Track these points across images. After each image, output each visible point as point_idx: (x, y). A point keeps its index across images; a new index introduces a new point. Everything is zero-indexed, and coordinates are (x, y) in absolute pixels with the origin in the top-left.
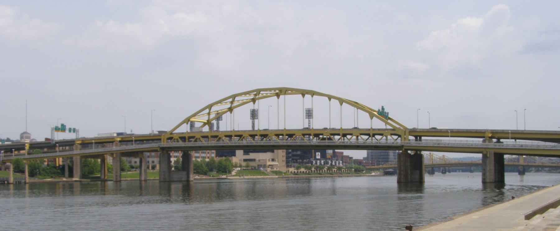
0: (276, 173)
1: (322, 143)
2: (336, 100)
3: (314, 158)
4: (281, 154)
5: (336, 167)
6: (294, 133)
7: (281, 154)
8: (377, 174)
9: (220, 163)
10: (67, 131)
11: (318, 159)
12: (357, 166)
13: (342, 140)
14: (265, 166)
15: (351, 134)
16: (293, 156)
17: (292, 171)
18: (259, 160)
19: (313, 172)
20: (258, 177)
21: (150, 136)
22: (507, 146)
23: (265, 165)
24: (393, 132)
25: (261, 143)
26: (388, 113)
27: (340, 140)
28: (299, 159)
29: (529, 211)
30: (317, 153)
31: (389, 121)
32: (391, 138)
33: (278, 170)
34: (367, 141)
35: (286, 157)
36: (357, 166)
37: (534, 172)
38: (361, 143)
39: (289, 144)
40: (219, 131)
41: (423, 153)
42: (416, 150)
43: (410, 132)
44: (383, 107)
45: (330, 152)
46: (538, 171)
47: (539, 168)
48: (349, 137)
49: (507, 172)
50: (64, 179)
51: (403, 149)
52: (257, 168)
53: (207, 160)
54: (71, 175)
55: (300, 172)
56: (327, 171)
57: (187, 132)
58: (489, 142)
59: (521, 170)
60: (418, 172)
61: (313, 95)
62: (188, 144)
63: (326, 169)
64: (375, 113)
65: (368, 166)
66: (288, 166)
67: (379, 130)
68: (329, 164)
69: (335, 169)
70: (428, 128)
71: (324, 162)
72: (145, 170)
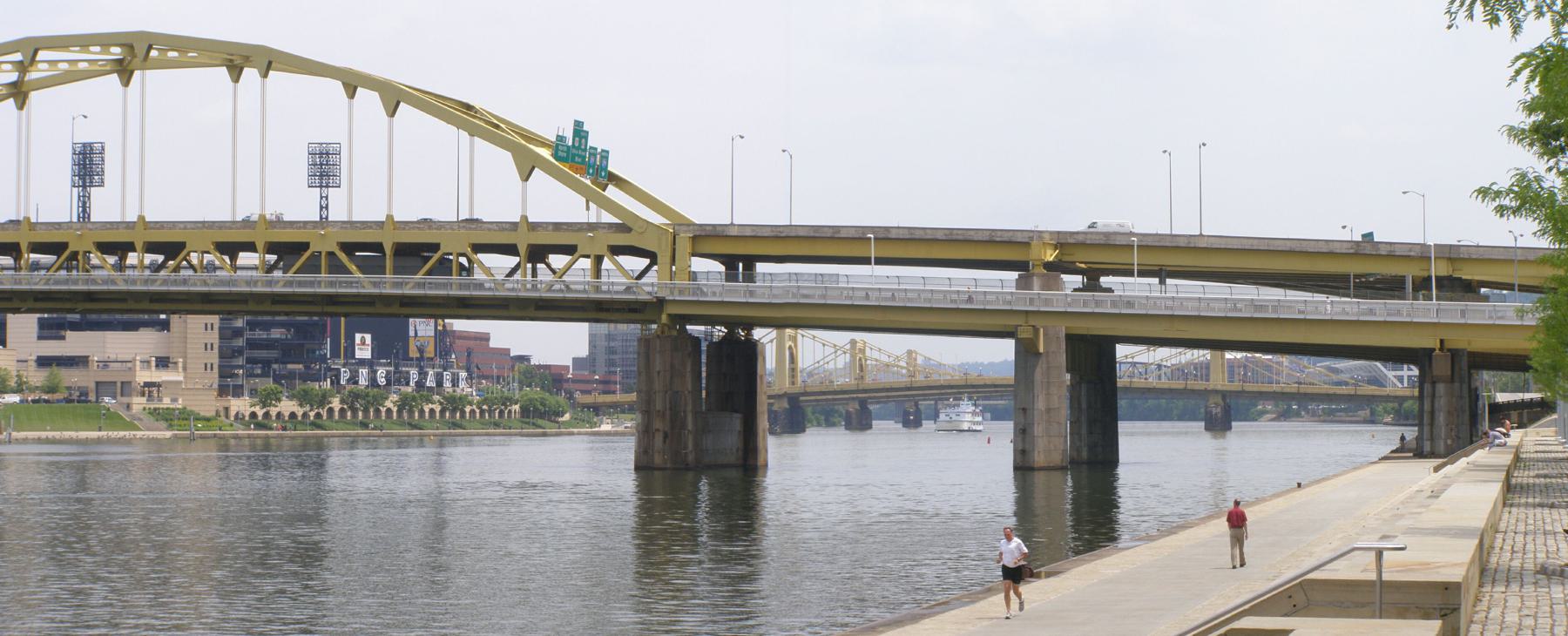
0: (167, 417)
1: (300, 284)
8: (621, 429)
11: (362, 362)
13: (525, 275)
14: (126, 388)
15: (569, 250)
16: (252, 345)
17: (242, 409)
18: (105, 364)
20: (83, 435)
22: (824, 297)
23: (129, 383)
25: (154, 281)
26: (605, 155)
27: (518, 276)
28: (276, 361)
29: (19, 359)
30: (358, 337)
31: (612, 192)
33: (180, 404)
34: (644, 280)
36: (535, 393)
41: (758, 333)
44: (578, 125)
45: (422, 329)
46: (1284, 415)
48: (557, 261)
51: (664, 318)
52: (92, 397)
55: (279, 415)
56: (400, 412)
58: (1046, 286)
59: (1217, 411)
60: (736, 421)
61: (269, 66)
64: (545, 153)
65: (589, 392)
66: (223, 391)
67: (558, 226)
69: (433, 406)
71: (387, 378)
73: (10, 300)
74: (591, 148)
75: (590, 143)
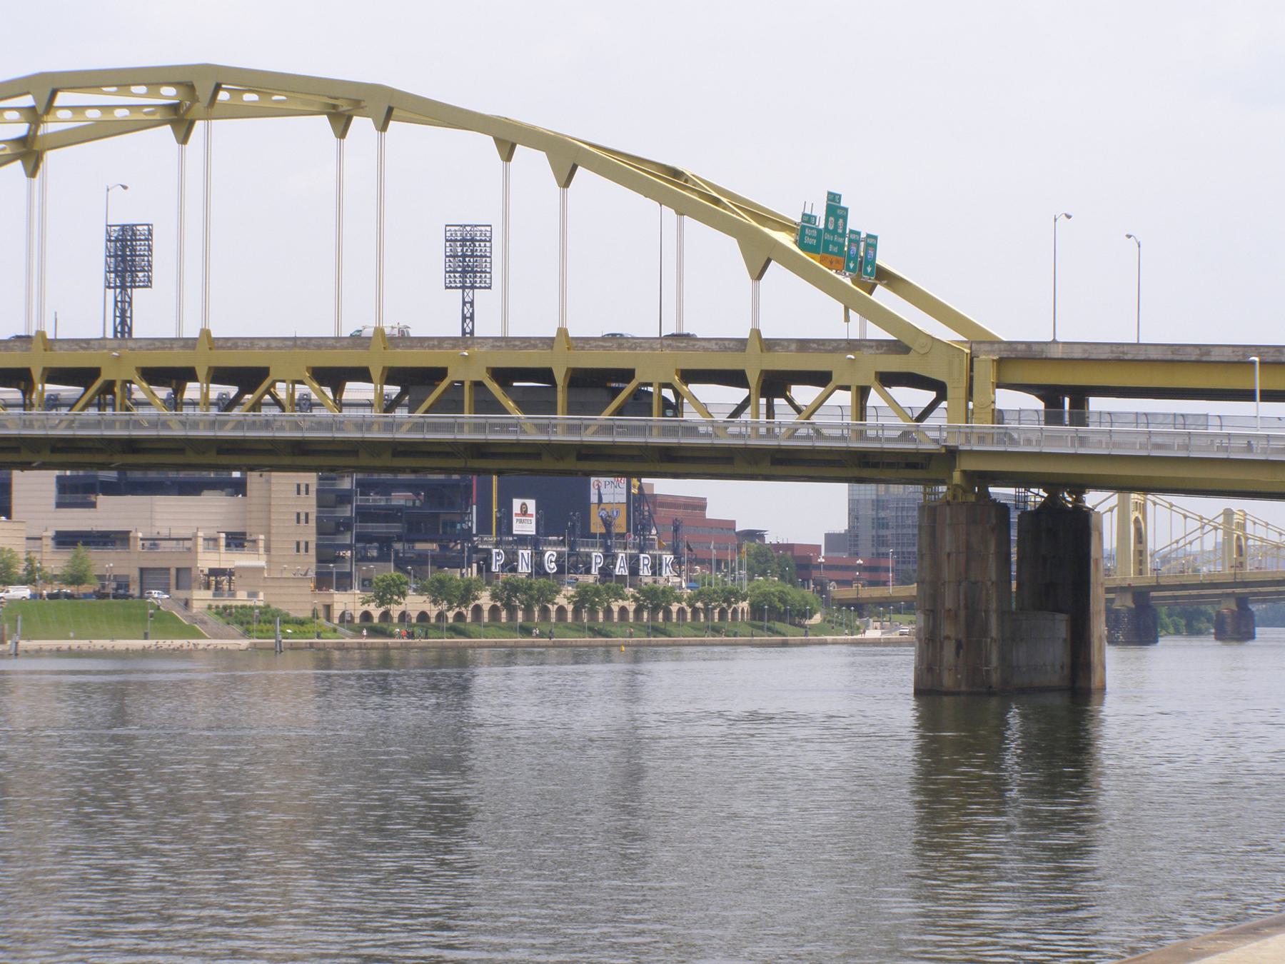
0: (242, 619)
1: (436, 427)
5: (630, 591)
8: (895, 636)
11: (523, 540)
12: (771, 584)
14: (183, 577)
15: (820, 378)
16: (365, 514)
17: (350, 608)
18: (153, 542)
19: (486, 615)
23: (189, 569)
24: (895, 364)
25: (223, 424)
26: (872, 242)
27: (746, 417)
28: (399, 538)
30: (517, 504)
33: (260, 601)
34: (928, 422)
36: (771, 584)
38: (888, 433)
39: (402, 435)
42: (1053, 484)
44: (833, 199)
48: (804, 394)
51: (957, 477)
55: (403, 616)
56: (577, 611)
60: (1061, 625)
64: (786, 239)
65: (848, 583)
66: (323, 582)
67: (804, 345)
68: (595, 571)
69: (625, 603)
70: (328, 331)
74: (852, 232)
75: (852, 224)
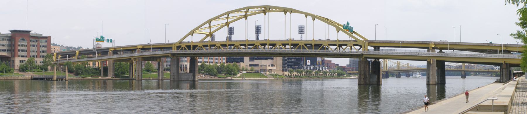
0: (273, 75)
1: (297, 51)
2: (310, 16)
3: (305, 64)
4: (279, 60)
6: (254, 43)
7: (279, 60)
8: (355, 77)
9: (228, 67)
10: (105, 41)
11: (308, 65)
12: (340, 71)
14: (265, 70)
15: (346, 45)
16: (288, 62)
18: (262, 66)
21: (164, 45)
22: (392, 53)
26: (352, 28)
27: (337, 50)
28: (293, 65)
30: (308, 61)
31: (354, 35)
32: (354, 48)
33: (275, 73)
35: (283, 63)
36: (340, 71)
37: (473, 76)
39: (293, 52)
40: (232, 41)
41: (380, 60)
42: (375, 58)
43: (369, 43)
45: (319, 59)
46: (476, 75)
47: (477, 73)
48: (344, 47)
49: (448, 75)
50: (100, 78)
51: (363, 57)
52: (259, 72)
53: (219, 65)
54: (106, 74)
56: (315, 74)
57: (209, 41)
60: (376, 76)
62: (192, 51)
63: (314, 73)
64: (342, 27)
65: (349, 71)
66: (283, 71)
67: (344, 41)
72: (162, 72)
73: (225, 54)
